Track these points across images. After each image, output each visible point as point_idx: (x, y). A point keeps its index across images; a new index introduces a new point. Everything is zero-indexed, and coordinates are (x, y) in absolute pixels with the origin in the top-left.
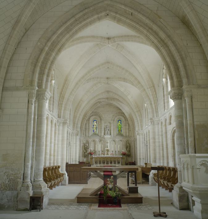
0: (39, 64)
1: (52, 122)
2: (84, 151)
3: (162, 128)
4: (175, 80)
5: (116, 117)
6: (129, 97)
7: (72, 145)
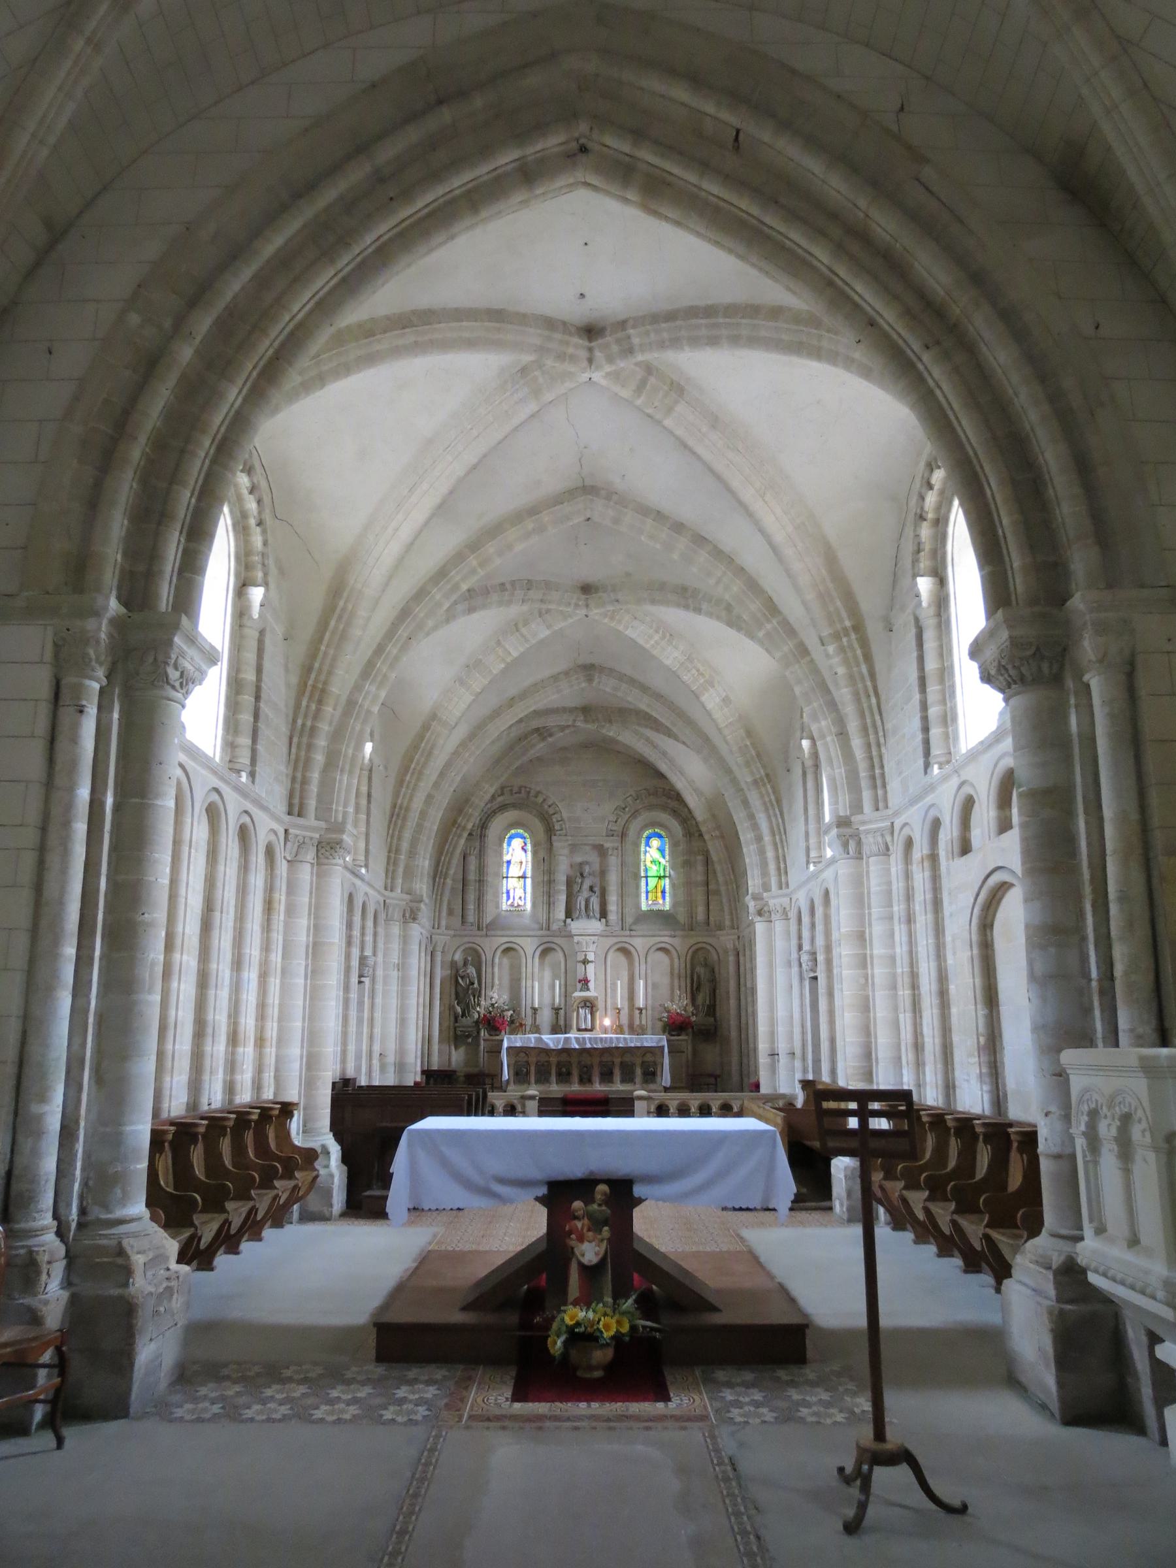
0: (136, 452)
1: (244, 834)
2: (451, 1008)
3: (908, 876)
4: (1016, 559)
5: (635, 814)
6: (711, 700)
7: (380, 972)
